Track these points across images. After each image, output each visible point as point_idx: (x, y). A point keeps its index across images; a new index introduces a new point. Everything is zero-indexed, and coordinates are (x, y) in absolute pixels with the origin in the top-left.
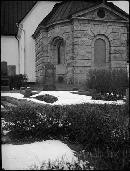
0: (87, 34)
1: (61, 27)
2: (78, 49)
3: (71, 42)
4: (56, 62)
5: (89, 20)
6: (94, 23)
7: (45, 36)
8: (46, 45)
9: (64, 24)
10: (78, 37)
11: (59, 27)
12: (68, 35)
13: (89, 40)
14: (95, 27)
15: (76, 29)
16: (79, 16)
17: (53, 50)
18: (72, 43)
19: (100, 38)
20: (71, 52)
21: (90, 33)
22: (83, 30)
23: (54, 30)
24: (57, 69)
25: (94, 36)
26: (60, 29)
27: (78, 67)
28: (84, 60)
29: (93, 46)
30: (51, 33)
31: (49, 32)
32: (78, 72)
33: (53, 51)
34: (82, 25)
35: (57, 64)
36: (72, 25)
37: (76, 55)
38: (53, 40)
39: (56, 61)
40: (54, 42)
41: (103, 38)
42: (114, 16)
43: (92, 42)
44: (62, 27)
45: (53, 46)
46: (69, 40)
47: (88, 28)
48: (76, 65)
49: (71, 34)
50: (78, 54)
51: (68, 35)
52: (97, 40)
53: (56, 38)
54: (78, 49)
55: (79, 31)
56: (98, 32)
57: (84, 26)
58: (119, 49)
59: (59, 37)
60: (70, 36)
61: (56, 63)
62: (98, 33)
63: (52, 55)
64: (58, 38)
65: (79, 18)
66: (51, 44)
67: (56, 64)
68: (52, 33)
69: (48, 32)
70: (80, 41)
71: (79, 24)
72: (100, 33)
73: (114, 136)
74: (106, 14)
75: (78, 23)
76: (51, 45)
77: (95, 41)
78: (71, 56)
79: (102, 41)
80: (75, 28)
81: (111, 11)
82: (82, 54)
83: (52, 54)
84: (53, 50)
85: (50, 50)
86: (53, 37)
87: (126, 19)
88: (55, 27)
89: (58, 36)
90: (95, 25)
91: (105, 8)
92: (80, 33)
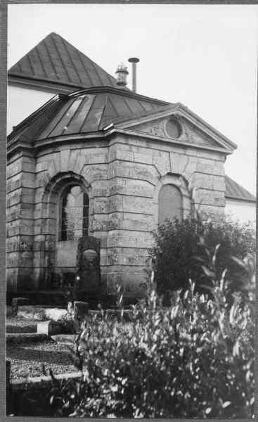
0: (145, 170)
1: (79, 151)
2: (124, 206)
3: (105, 188)
4: (57, 235)
5: (149, 140)
6: (159, 148)
7: (29, 168)
8: (31, 190)
9: (86, 144)
10: (126, 175)
11: (71, 150)
12: (98, 169)
13: (150, 185)
14: (160, 156)
15: (122, 158)
16: (222, 147)
17: (50, 203)
18: (108, 191)
19: (170, 182)
20: (104, 211)
21: (150, 169)
22: (136, 160)
23: (55, 154)
24: (59, 252)
25: (160, 178)
26: (74, 154)
27: (125, 249)
28: (138, 233)
29: (156, 197)
30: (46, 163)
31: (40, 160)
32: (125, 261)
33: (50, 207)
34: (134, 149)
35: (59, 241)
36: (109, 147)
37: (120, 220)
38: (53, 180)
39: (58, 231)
40: (54, 186)
41: (178, 182)
42: (199, 135)
43: (154, 190)
44: (80, 149)
45: (49, 195)
46: (99, 183)
47: (145, 157)
48: (121, 244)
49: (104, 167)
50: (125, 217)
51: (98, 169)
52: (164, 186)
53: (60, 174)
54: (125, 205)
55: (128, 164)
56: (168, 168)
57: (138, 153)
58: (211, 210)
59: (71, 173)
60: (102, 173)
61: (57, 237)
62: (169, 171)
63: (47, 217)
64: (68, 176)
65: (128, 132)
66: (46, 190)
67: (57, 240)
68: (50, 161)
69: (36, 158)
70: (129, 186)
71: (127, 147)
72: (172, 172)
73: (175, 379)
74: (184, 131)
75: (126, 144)
76: (47, 191)
77: (161, 189)
78: (104, 222)
79: (174, 191)
80: (119, 155)
81: (195, 123)
82: (135, 217)
83: (47, 214)
84: (50, 203)
85: (41, 204)
86: (52, 173)
87: (222, 144)
88: (60, 148)
89: (70, 170)
90: (162, 153)
91: (183, 117)
92: (128, 167)
